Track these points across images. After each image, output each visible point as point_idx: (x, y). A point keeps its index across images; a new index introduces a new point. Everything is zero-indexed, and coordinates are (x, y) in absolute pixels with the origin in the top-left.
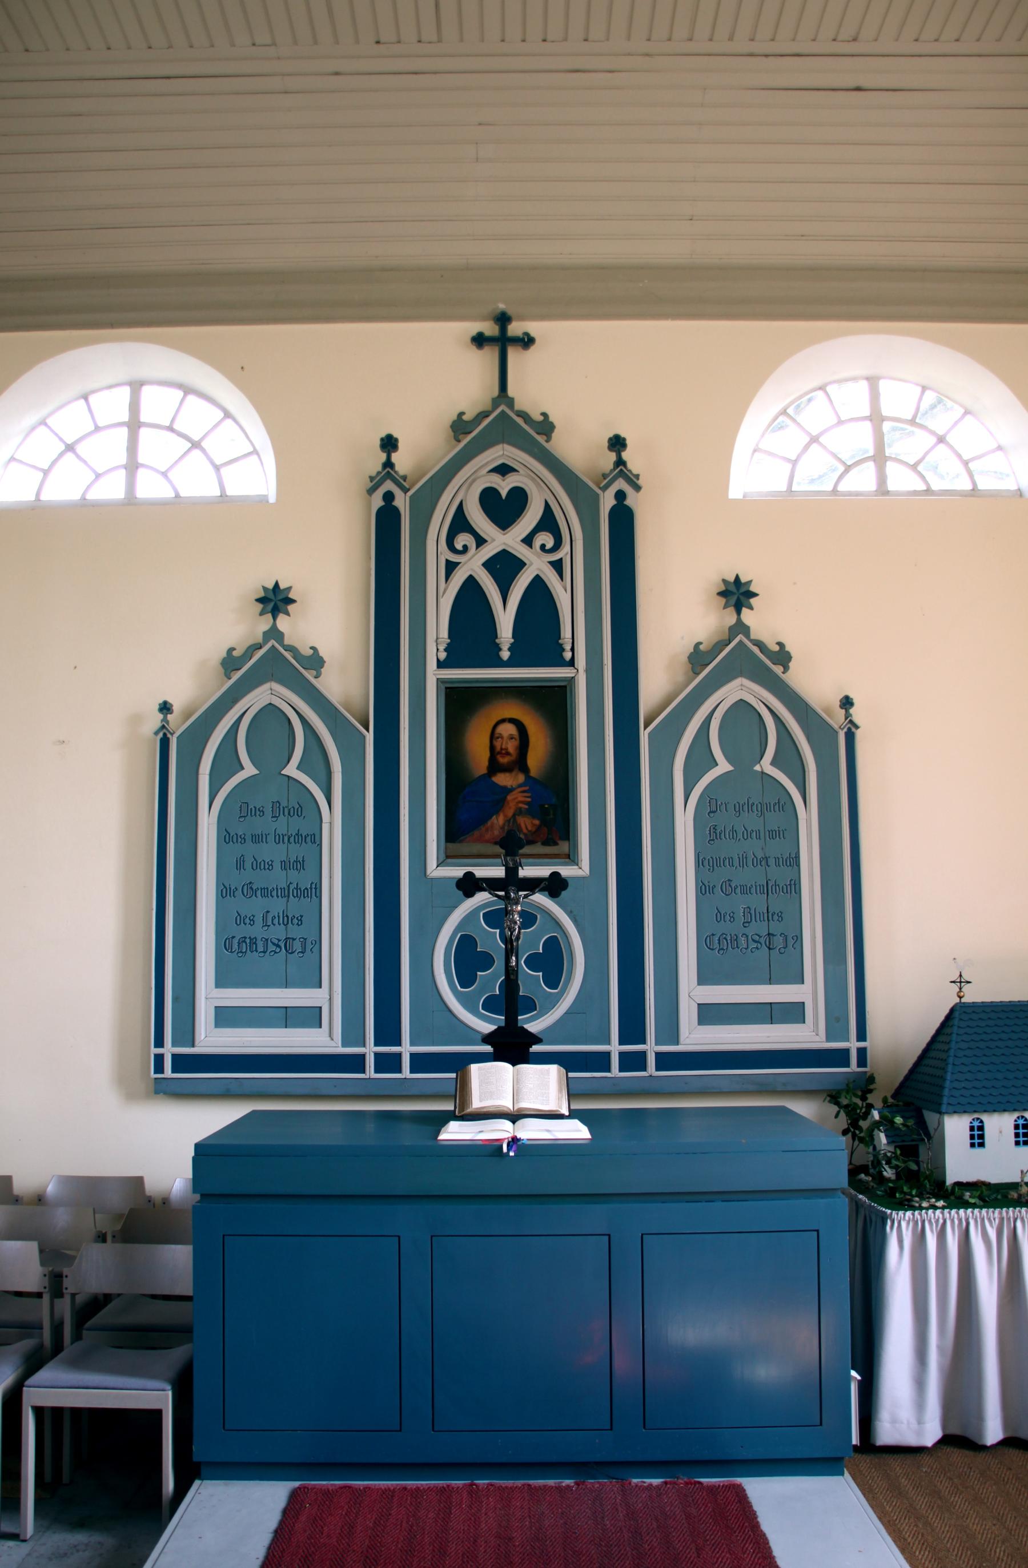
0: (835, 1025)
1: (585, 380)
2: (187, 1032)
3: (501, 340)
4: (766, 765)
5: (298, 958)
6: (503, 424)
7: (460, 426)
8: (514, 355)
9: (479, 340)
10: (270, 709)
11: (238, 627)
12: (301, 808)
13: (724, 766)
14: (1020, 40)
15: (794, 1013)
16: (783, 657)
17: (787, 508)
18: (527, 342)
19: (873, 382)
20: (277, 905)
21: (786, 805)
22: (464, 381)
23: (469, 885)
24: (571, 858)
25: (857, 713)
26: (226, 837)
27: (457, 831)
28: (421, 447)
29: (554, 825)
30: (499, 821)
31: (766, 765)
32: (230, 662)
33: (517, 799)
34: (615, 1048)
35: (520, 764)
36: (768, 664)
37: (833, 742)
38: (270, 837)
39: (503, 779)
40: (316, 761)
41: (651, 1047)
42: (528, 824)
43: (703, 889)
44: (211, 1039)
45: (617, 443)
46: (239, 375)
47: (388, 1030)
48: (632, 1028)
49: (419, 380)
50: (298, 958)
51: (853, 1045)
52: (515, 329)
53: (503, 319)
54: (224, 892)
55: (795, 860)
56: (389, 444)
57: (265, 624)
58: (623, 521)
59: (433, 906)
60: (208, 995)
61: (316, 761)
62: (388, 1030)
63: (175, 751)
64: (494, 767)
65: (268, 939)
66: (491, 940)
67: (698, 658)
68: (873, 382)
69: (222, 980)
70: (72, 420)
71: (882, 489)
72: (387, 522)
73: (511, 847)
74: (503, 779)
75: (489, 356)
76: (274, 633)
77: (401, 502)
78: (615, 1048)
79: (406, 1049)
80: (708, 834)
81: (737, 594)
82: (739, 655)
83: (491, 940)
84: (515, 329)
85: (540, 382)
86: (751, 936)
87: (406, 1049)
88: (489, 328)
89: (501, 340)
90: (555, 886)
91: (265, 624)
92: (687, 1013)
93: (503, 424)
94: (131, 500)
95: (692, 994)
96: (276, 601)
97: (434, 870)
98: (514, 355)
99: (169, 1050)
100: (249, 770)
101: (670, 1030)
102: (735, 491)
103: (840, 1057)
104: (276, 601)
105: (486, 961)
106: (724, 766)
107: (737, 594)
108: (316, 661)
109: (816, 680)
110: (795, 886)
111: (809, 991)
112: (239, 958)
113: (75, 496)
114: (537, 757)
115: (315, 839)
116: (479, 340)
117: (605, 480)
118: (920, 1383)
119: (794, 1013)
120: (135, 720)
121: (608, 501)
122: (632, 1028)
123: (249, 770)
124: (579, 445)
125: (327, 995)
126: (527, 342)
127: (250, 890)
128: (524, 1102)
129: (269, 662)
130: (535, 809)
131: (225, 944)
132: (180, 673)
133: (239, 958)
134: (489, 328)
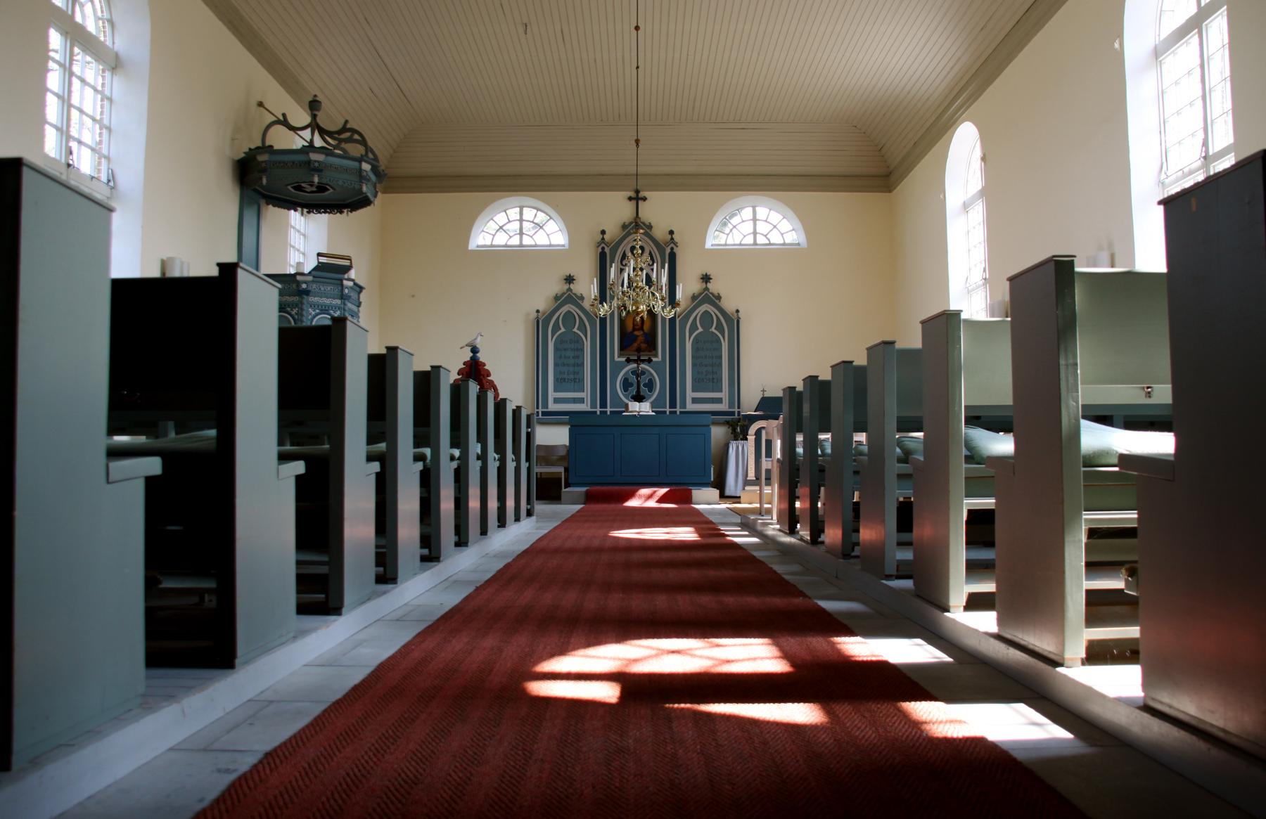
0: (731, 404)
1: (662, 210)
2: (546, 405)
3: (637, 198)
4: (713, 329)
5: (578, 384)
6: (636, 225)
7: (624, 227)
8: (640, 202)
9: (630, 199)
10: (569, 312)
11: (558, 287)
12: (578, 341)
13: (701, 330)
14: (219, 771)
15: (719, 401)
16: (719, 297)
17: (725, 254)
18: (645, 199)
19: (754, 208)
20: (571, 369)
21: (718, 341)
22: (624, 211)
23: (628, 361)
24: (656, 356)
25: (740, 314)
26: (556, 349)
27: (623, 348)
28: (613, 232)
29: (651, 344)
30: (635, 345)
31: (713, 329)
32: (557, 298)
33: (641, 339)
34: (668, 410)
35: (642, 328)
36: (714, 300)
37: (733, 323)
38: (569, 350)
39: (636, 333)
40: (583, 328)
41: (678, 410)
42: (643, 346)
43: (694, 365)
44: (552, 407)
45: (671, 232)
46: (556, 207)
47: (603, 405)
48: (673, 405)
49: (612, 210)
50: (578, 384)
51: (736, 410)
52: (642, 194)
53: (637, 192)
54: (556, 365)
55: (721, 357)
56: (603, 232)
57: (566, 287)
58: (673, 257)
59: (617, 368)
60: (552, 394)
61: (583, 328)
62: (603, 405)
63: (541, 324)
64: (634, 329)
65: (569, 379)
66: (633, 379)
67: (694, 297)
68: (754, 208)
69: (556, 390)
70: (501, 218)
71: (755, 243)
72: (602, 256)
73: (639, 350)
74: (636, 333)
75: (634, 202)
76: (569, 289)
77: (607, 250)
78: (668, 410)
79: (609, 410)
80: (696, 349)
81: (706, 278)
82: (707, 297)
83: (633, 379)
84: (642, 194)
85: (648, 212)
86: (707, 378)
87: (609, 410)
88: (632, 194)
89: (637, 198)
90: (650, 361)
91: (566, 287)
92: (689, 400)
93: (636, 225)
94: (521, 245)
95: (690, 394)
96: (570, 279)
97: (617, 359)
98: (640, 202)
99: (540, 410)
100: (563, 330)
101: (684, 404)
102: (708, 245)
103: (732, 413)
104: (570, 279)
105: (631, 385)
106: (701, 330)
107: (706, 278)
108: (582, 298)
109: (729, 304)
110: (720, 365)
111: (724, 394)
112: (561, 384)
113: (503, 243)
114: (646, 327)
115: (583, 350)
116: (630, 199)
117: (667, 244)
118: (736, 481)
119: (719, 401)
120: (528, 314)
121: (668, 251)
122: (673, 405)
123: (563, 330)
124: (660, 233)
125: (586, 394)
126: (645, 199)
127: (564, 365)
128: (644, 408)
129: (568, 298)
130: (646, 342)
131: (556, 380)
132: (540, 300)
133: (561, 384)
134: (632, 194)
